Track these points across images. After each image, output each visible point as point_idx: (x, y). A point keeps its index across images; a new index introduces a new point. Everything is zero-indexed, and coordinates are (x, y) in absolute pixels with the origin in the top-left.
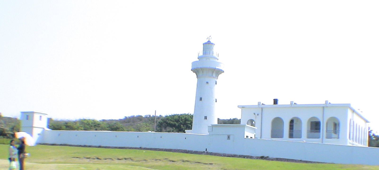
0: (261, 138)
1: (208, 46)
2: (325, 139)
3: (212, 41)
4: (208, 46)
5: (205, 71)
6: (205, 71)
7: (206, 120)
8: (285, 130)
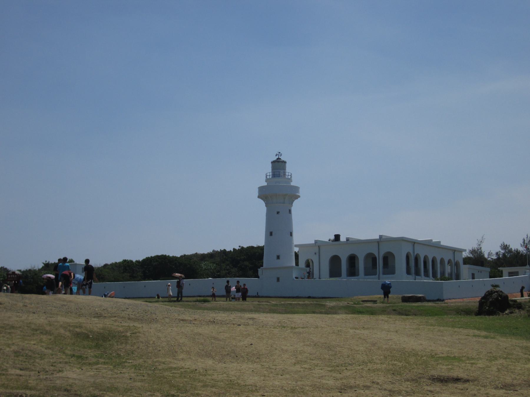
0: (319, 278)
1: (278, 165)
2: (381, 275)
3: (283, 158)
4: (278, 165)
5: (278, 195)
6: (278, 195)
7: (278, 260)
8: (342, 267)
